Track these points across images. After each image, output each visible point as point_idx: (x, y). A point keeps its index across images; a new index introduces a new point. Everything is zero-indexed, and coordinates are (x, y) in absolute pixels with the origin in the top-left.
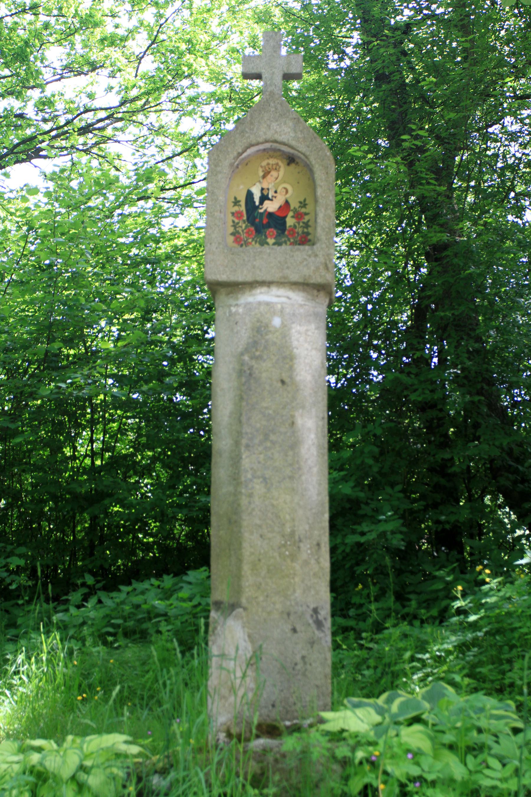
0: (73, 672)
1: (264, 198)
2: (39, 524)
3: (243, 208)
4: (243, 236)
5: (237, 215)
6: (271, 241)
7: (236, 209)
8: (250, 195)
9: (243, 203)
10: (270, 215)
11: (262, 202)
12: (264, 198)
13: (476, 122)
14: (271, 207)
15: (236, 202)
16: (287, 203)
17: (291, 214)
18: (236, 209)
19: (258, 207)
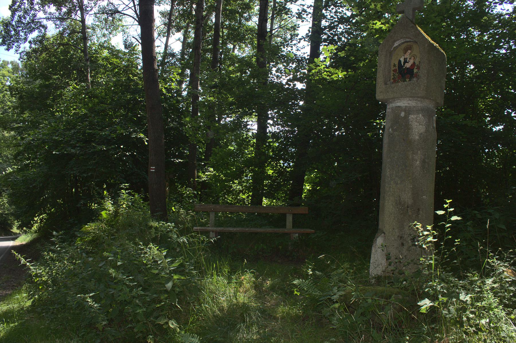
0: (386, 29)
1: (405, 62)
2: (257, 201)
3: (397, 68)
4: (397, 79)
5: (395, 71)
6: (407, 80)
7: (395, 68)
8: (400, 61)
9: (397, 66)
10: (407, 69)
11: (404, 64)
12: (405, 62)
13: (425, 240)
14: (408, 65)
15: (395, 65)
16: (414, 63)
17: (416, 67)
18: (395, 68)
19: (403, 66)
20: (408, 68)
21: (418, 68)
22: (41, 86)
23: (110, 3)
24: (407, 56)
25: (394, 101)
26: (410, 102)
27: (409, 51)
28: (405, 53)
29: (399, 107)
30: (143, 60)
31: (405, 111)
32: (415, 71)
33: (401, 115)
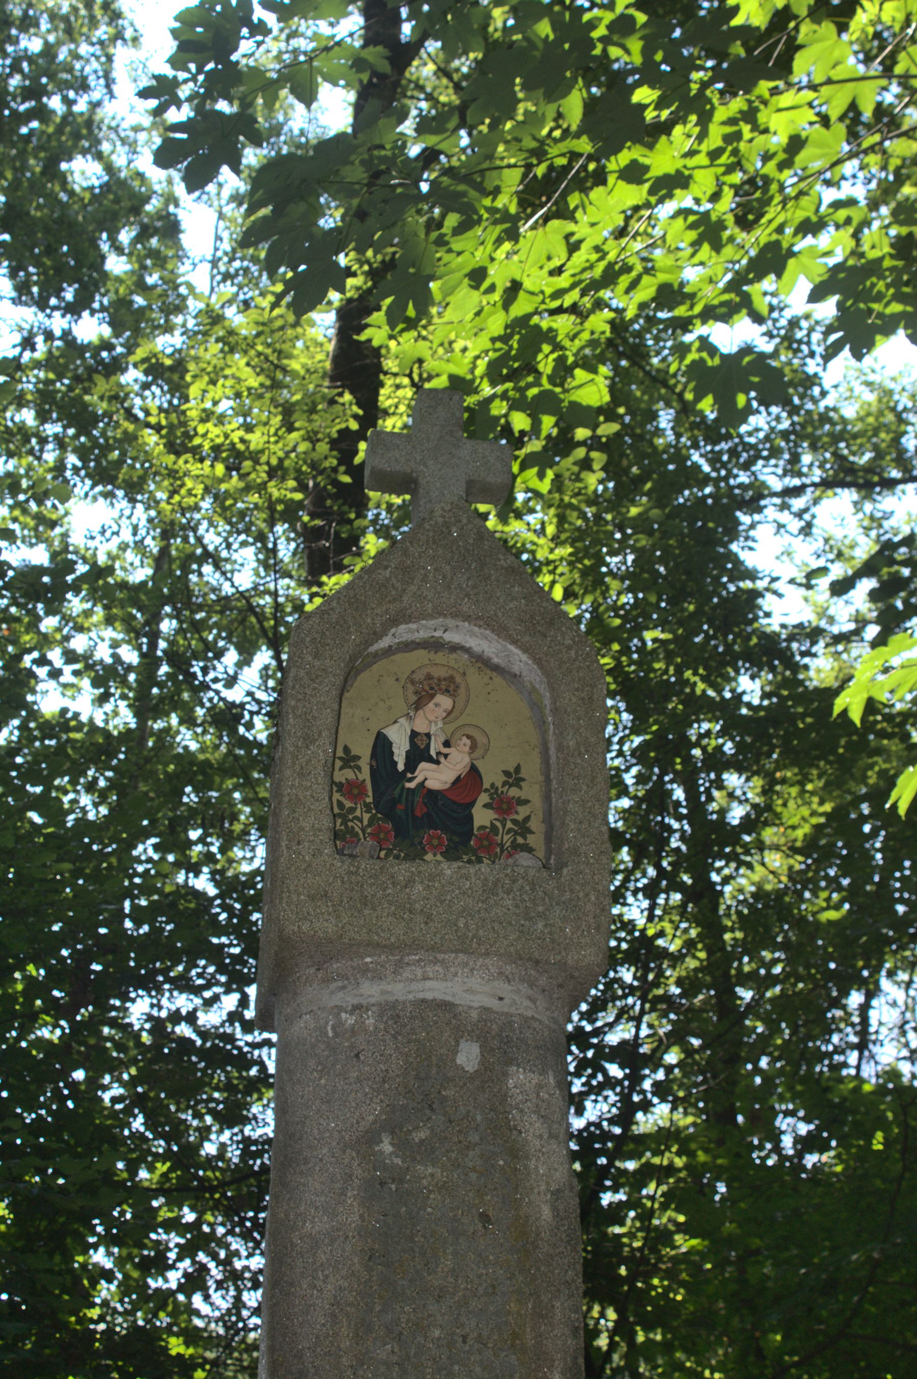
1: (419, 753)
3: (365, 775)
7: (349, 774)
9: (365, 764)
12: (419, 753)
14: (436, 777)
15: (350, 760)
17: (484, 798)
20: (432, 793)
21: (502, 805)
22: (873, 596)
23: (851, 397)
24: (431, 719)
25: (400, 965)
26: (503, 988)
27: (444, 702)
28: (418, 705)
29: (445, 1006)
30: (383, 492)
31: (481, 1035)
32: (482, 817)
33: (461, 1059)
